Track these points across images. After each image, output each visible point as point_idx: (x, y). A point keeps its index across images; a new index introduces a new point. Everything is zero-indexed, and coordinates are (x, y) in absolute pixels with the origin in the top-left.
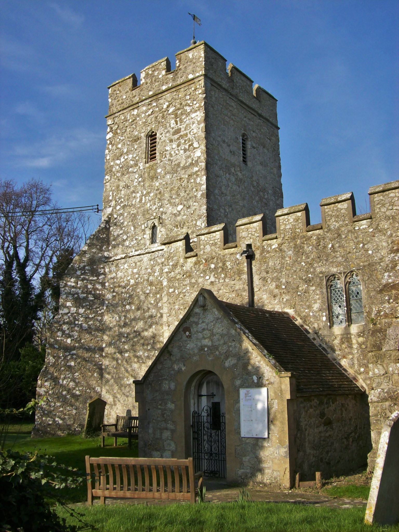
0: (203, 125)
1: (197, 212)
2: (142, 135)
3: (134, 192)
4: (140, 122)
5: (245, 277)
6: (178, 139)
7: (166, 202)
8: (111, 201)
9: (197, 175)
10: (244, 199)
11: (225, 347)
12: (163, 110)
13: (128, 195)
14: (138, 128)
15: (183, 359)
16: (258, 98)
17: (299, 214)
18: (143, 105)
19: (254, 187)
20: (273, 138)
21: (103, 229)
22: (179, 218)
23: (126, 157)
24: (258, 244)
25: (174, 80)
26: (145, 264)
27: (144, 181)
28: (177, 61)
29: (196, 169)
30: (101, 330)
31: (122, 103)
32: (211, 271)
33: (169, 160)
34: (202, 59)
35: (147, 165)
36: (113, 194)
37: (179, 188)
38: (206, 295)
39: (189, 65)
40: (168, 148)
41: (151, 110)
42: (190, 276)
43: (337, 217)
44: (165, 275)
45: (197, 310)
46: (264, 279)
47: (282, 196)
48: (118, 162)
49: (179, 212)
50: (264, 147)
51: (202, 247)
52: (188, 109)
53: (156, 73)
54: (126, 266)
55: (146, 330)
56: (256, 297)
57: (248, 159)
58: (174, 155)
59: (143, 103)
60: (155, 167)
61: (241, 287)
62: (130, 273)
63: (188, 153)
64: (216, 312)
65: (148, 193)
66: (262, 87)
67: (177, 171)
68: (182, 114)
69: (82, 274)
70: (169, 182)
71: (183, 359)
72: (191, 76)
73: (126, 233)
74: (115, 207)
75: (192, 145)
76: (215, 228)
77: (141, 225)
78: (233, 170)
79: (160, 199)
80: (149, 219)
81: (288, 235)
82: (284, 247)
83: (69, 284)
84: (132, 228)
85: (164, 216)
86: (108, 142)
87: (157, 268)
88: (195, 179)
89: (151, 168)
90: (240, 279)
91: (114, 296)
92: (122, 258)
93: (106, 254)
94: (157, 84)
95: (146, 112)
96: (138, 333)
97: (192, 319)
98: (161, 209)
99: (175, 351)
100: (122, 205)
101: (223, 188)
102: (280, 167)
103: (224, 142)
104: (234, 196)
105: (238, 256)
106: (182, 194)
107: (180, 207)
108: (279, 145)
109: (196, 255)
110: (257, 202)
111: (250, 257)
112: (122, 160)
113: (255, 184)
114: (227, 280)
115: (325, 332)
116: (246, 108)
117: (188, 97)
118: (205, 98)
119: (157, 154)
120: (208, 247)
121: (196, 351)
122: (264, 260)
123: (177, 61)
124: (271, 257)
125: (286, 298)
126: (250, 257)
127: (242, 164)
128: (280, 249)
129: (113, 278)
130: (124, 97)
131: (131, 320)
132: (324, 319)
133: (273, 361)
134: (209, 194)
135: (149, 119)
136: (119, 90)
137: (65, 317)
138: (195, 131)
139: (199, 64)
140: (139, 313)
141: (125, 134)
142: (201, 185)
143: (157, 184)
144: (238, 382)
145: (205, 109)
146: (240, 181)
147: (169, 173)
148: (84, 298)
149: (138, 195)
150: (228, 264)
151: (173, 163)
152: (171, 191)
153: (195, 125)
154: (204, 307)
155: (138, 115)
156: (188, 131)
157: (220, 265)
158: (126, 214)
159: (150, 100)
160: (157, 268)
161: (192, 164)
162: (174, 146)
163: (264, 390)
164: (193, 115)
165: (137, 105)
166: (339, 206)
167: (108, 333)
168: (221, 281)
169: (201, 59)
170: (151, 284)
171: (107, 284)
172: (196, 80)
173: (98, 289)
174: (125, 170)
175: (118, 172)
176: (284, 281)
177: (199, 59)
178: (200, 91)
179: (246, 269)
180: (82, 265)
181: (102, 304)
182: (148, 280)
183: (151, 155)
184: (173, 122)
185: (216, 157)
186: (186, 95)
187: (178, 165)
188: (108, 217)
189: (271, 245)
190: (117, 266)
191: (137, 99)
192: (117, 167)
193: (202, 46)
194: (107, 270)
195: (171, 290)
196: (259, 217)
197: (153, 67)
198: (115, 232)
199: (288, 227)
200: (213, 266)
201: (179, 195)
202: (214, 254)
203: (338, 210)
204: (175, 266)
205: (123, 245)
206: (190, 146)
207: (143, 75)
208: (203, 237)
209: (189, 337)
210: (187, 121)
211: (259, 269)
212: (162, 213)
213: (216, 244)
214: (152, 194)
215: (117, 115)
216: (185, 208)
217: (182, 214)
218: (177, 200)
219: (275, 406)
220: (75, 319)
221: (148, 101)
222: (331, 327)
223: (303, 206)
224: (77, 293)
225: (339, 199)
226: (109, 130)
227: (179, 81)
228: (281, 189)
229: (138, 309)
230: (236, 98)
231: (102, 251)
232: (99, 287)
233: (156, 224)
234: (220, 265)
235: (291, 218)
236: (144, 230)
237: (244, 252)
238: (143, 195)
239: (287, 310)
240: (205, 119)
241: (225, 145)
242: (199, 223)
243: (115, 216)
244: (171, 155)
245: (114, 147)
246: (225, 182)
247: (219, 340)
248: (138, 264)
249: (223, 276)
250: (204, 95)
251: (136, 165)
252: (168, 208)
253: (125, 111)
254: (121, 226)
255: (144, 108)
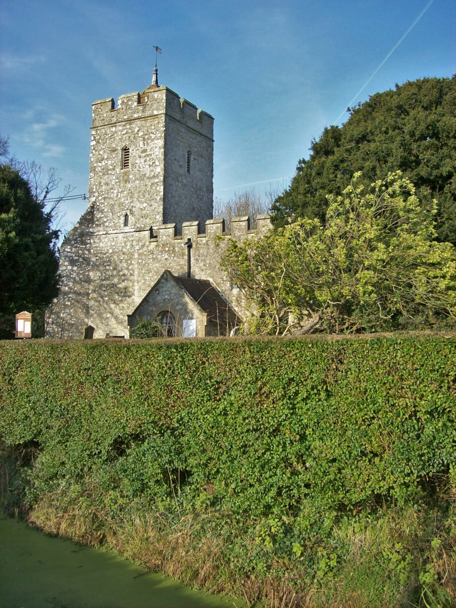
0: (162, 150)
1: (156, 210)
2: (119, 148)
3: (112, 189)
4: (117, 138)
5: (186, 257)
6: (145, 156)
7: (135, 199)
8: (95, 192)
9: (158, 185)
10: (186, 198)
11: (176, 300)
12: (135, 133)
13: (108, 190)
14: (115, 142)
15: (155, 305)
16: (200, 121)
17: (219, 225)
18: (120, 126)
19: (193, 188)
20: (209, 149)
21: (89, 212)
22: (144, 212)
23: (106, 162)
24: (195, 239)
25: (143, 111)
26: (120, 240)
27: (119, 182)
28: (146, 98)
29: (157, 180)
30: (88, 282)
31: (103, 120)
32: (166, 252)
33: (138, 170)
34: (164, 101)
35: (122, 171)
36: (96, 187)
37: (144, 191)
38: (168, 274)
39: (155, 103)
40: (137, 161)
41: (126, 131)
42: (152, 253)
43: (239, 229)
44: (136, 251)
45: (163, 281)
46: (197, 260)
47: (213, 192)
48: (100, 164)
49: (145, 208)
50: (202, 157)
51: (161, 236)
52: (153, 136)
53: (130, 103)
54: (106, 240)
55: (120, 283)
56: (192, 270)
57: (191, 168)
58: (141, 167)
59: (120, 124)
60: (128, 174)
61: (184, 263)
62: (109, 245)
63: (152, 168)
64: (173, 283)
65: (123, 191)
66: (204, 110)
67: (143, 180)
68: (148, 139)
69: (75, 243)
70: (138, 186)
71: (155, 305)
72: (155, 112)
73: (106, 217)
74: (98, 197)
75: (154, 163)
76: (169, 225)
77: (117, 213)
78: (180, 179)
79: (131, 197)
80: (123, 210)
81: (212, 236)
82: (210, 243)
83: (66, 250)
84: (111, 214)
85: (134, 209)
86: (92, 148)
87: (129, 244)
88: (156, 187)
89: (125, 173)
90: (183, 259)
91: (97, 260)
92: (103, 234)
93: (91, 230)
94: (130, 111)
95: (122, 131)
96: (114, 285)
97: (160, 285)
98: (132, 204)
99: (151, 300)
100: (103, 196)
101: (174, 192)
102: (212, 170)
103: (176, 159)
104: (180, 197)
105: (183, 245)
106: (147, 196)
107: (145, 205)
108: (213, 154)
109: (157, 241)
110: (195, 199)
111: (190, 247)
112: (103, 164)
113: (194, 186)
114: (175, 258)
115: (227, 292)
116: (192, 131)
117: (153, 127)
118: (165, 130)
119: (130, 164)
120: (164, 237)
121: (162, 301)
122: (197, 249)
123: (146, 98)
124: (202, 247)
125: (209, 272)
126: (190, 247)
127: (187, 174)
128: (207, 244)
129: (97, 247)
130: (105, 115)
131: (110, 276)
132: (228, 285)
133: (199, 308)
134: (165, 198)
135: (124, 137)
136: (100, 108)
137: (65, 272)
138: (157, 153)
139: (161, 104)
140: (115, 272)
141: (106, 145)
142: (160, 192)
143: (129, 186)
144: (182, 317)
145: (165, 139)
146: (185, 185)
147: (138, 179)
148: (77, 260)
149: (115, 191)
150: (176, 248)
151: (141, 173)
152: (139, 192)
153: (157, 149)
154: (166, 279)
155: (116, 132)
156: (152, 153)
157: (172, 248)
158: (106, 204)
159: (125, 123)
160: (129, 244)
161: (154, 176)
162: (142, 161)
163: (194, 321)
164: (156, 142)
165: (115, 125)
166: (241, 223)
167: (92, 284)
168: (172, 258)
169: (163, 101)
170: (124, 253)
171: (92, 251)
172: (159, 116)
173: (86, 254)
174: (106, 171)
175: (100, 172)
176: (208, 262)
177: (162, 100)
178: (162, 125)
179: (187, 253)
180: (75, 237)
181: (88, 264)
182: (122, 251)
183: (125, 164)
184: (141, 143)
185: (170, 172)
186: (151, 125)
187: (145, 175)
188: (92, 204)
189: (202, 241)
190: (99, 239)
191: (114, 120)
192: (100, 168)
193: (165, 91)
194: (92, 241)
195: (140, 261)
196: (196, 223)
197: (128, 97)
198: (98, 215)
199: (212, 231)
200: (167, 249)
201: (144, 196)
202: (168, 242)
203: (241, 226)
204: (143, 246)
205: (104, 226)
206: (153, 163)
207: (120, 102)
208: (161, 230)
209: (158, 294)
210: (152, 145)
211: (195, 254)
212: (132, 207)
213: (169, 236)
214: (125, 193)
215: (99, 128)
216: (148, 206)
217: (146, 209)
218: (143, 200)
219: (200, 327)
220: (71, 274)
221: (123, 123)
222: (231, 290)
223: (222, 220)
224: (72, 257)
225: (241, 220)
226: (92, 138)
227: (147, 113)
228: (212, 187)
229: (114, 269)
230: (185, 125)
231: (89, 227)
232: (87, 252)
233: (128, 214)
234: (172, 248)
235: (215, 226)
236: (119, 217)
237: (186, 243)
238: (119, 192)
239: (208, 279)
240: (164, 146)
241: (176, 162)
242: (157, 217)
243: (98, 204)
244: (140, 167)
245: (97, 153)
246: (175, 188)
247: (174, 296)
248: (115, 239)
249: (173, 255)
250: (164, 129)
251: (114, 169)
252: (136, 204)
253: (105, 127)
254: (102, 211)
255: (121, 128)
